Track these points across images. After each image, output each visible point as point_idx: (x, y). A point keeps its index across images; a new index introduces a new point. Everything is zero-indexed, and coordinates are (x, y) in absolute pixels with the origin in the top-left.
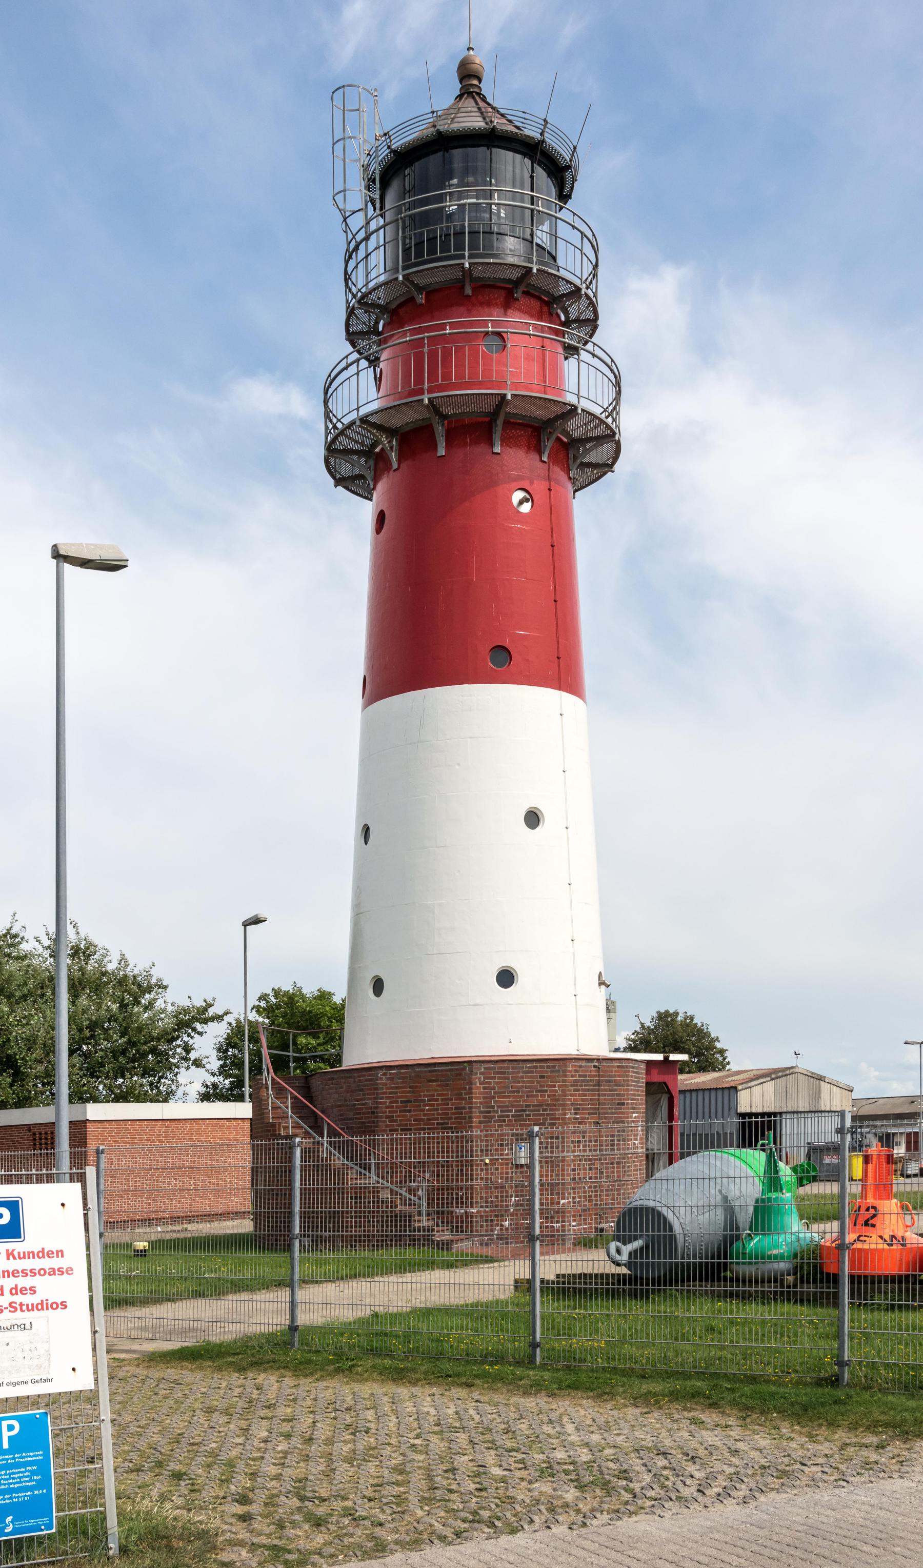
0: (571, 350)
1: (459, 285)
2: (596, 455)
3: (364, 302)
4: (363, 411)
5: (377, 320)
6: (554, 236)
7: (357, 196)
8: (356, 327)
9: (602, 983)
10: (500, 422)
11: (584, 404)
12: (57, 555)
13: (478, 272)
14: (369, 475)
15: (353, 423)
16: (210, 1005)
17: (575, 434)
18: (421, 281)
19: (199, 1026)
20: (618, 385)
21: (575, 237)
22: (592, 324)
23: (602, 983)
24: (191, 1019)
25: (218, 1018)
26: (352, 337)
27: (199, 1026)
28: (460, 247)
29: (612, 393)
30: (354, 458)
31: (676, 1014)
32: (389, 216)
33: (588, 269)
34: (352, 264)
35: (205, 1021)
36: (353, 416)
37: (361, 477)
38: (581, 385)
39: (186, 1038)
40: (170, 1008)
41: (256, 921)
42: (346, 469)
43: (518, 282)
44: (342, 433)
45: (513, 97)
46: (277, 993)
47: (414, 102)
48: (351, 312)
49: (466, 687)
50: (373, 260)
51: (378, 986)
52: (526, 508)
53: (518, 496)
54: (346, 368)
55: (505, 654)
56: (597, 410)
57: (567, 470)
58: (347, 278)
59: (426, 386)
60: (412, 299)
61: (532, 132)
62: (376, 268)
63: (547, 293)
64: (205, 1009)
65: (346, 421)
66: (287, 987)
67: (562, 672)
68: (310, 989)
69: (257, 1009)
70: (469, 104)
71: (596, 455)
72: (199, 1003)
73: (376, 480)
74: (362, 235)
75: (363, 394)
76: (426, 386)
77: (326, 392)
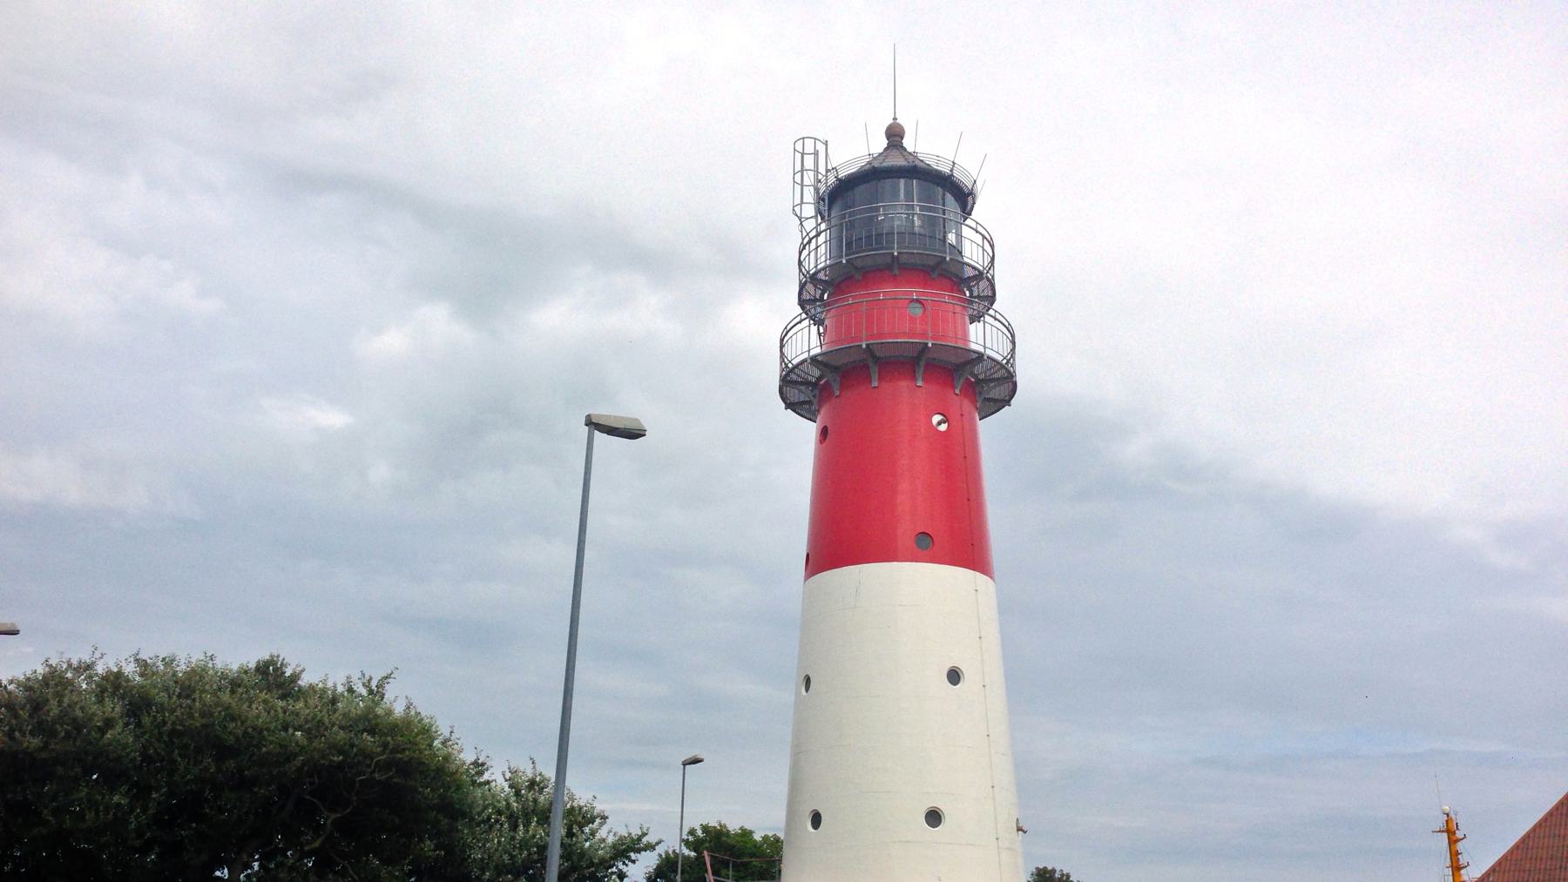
0: (975, 319)
1: (889, 267)
2: (997, 392)
3: (813, 278)
4: (813, 353)
5: (822, 293)
6: (959, 236)
7: (809, 210)
8: (806, 296)
9: (1019, 829)
10: (922, 363)
11: (989, 352)
12: (593, 424)
13: (904, 259)
14: (815, 401)
15: (804, 361)
16: (644, 834)
17: (982, 377)
18: (859, 263)
19: (633, 856)
20: (1013, 343)
21: (979, 239)
22: (992, 299)
23: (1019, 829)
24: (627, 848)
25: (650, 847)
26: (802, 303)
27: (633, 856)
29: (1010, 346)
30: (802, 389)
31: (1054, 871)
32: (833, 222)
33: (987, 260)
34: (805, 253)
35: (639, 851)
36: (805, 356)
37: (809, 403)
38: (982, 337)
39: (621, 866)
40: (611, 839)
41: (696, 761)
42: (795, 395)
43: (934, 268)
44: (792, 370)
45: (926, 146)
46: (705, 829)
47: (854, 148)
48: (802, 287)
49: (895, 564)
50: (822, 250)
51: (816, 820)
52: (943, 427)
53: (936, 418)
55: (928, 540)
56: (1000, 358)
57: (974, 402)
58: (800, 263)
59: (864, 334)
60: (852, 277)
61: (945, 169)
62: (819, 257)
63: (957, 276)
64: (640, 839)
65: (795, 362)
66: (713, 823)
68: (733, 826)
69: (687, 843)
70: (895, 152)
71: (997, 392)
72: (635, 832)
73: (820, 406)
74: (813, 234)
75: (808, 342)
76: (864, 334)
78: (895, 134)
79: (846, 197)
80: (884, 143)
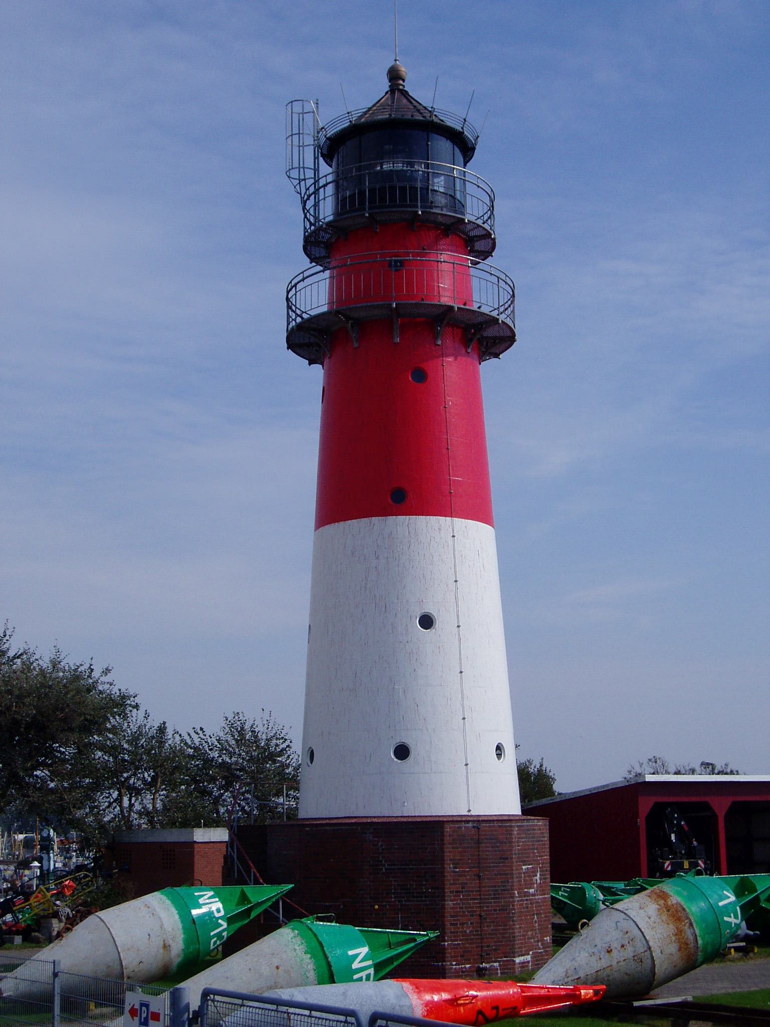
28: (414, 199)
38: (484, 298)
47: (357, 95)
54: (303, 280)
67: (480, 512)
75: (317, 297)
77: (288, 292)
78: (394, 76)
79: (350, 145)
80: (385, 85)
